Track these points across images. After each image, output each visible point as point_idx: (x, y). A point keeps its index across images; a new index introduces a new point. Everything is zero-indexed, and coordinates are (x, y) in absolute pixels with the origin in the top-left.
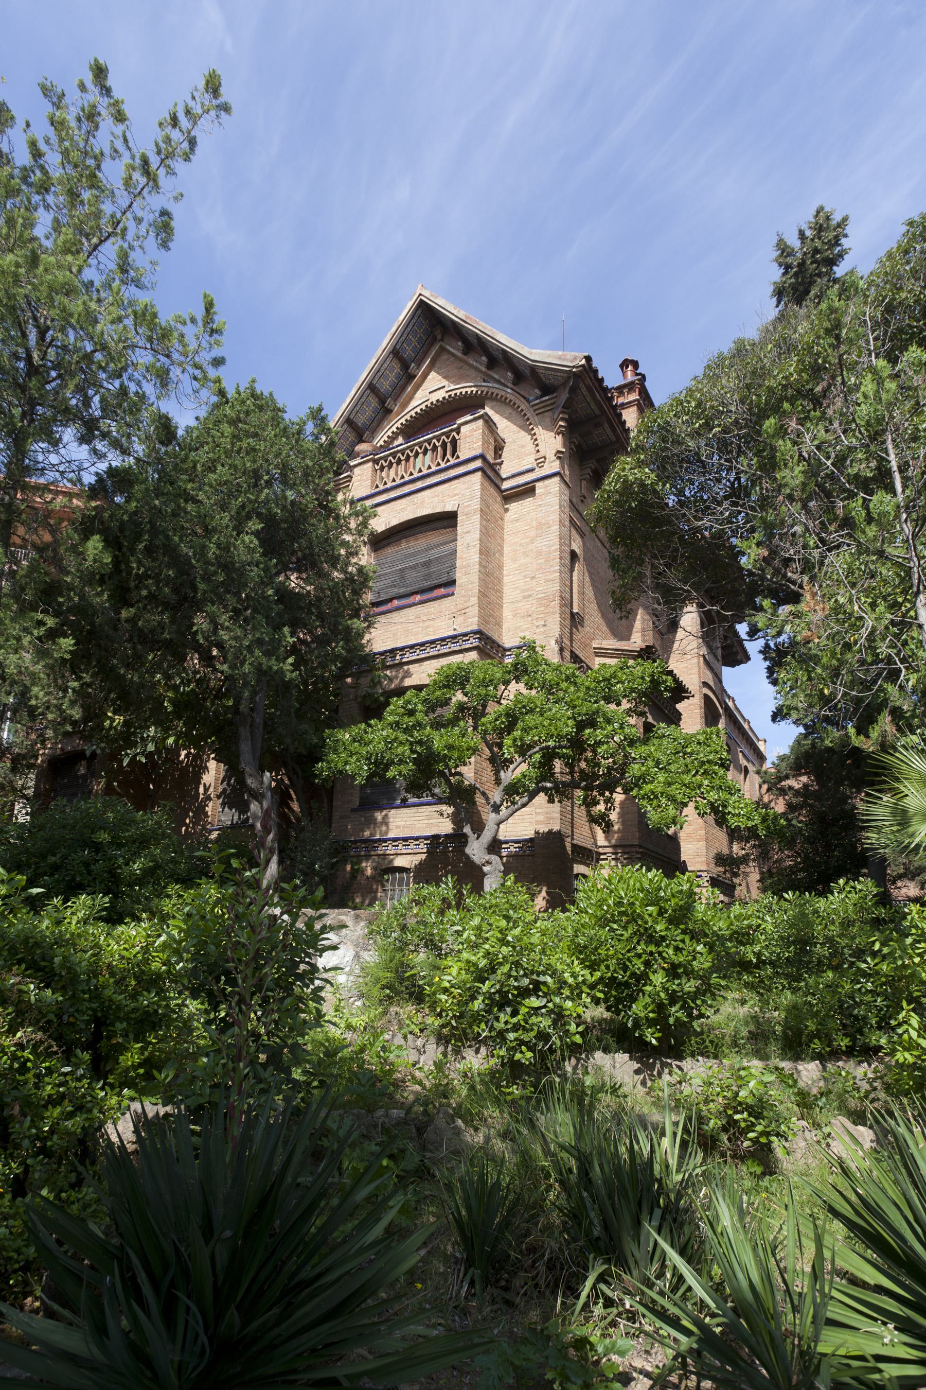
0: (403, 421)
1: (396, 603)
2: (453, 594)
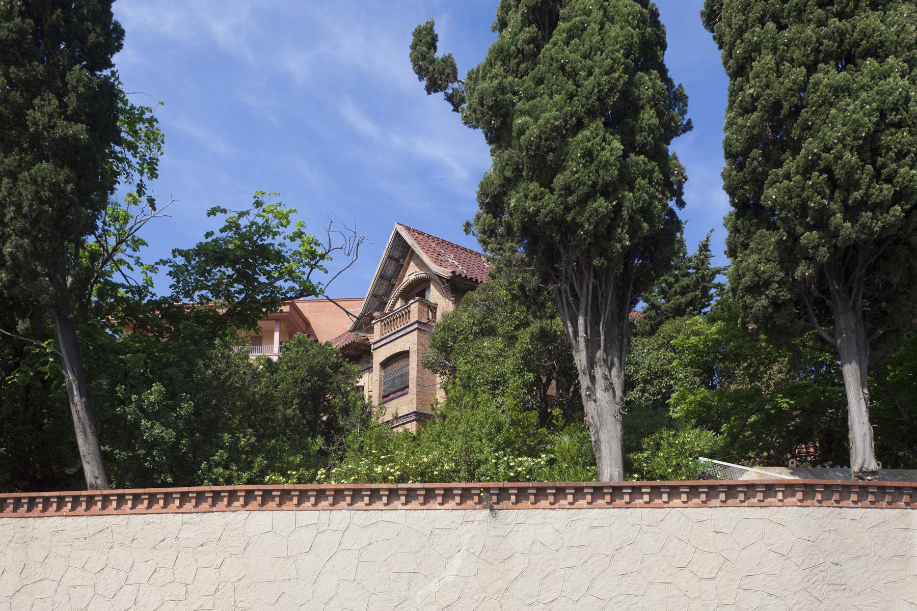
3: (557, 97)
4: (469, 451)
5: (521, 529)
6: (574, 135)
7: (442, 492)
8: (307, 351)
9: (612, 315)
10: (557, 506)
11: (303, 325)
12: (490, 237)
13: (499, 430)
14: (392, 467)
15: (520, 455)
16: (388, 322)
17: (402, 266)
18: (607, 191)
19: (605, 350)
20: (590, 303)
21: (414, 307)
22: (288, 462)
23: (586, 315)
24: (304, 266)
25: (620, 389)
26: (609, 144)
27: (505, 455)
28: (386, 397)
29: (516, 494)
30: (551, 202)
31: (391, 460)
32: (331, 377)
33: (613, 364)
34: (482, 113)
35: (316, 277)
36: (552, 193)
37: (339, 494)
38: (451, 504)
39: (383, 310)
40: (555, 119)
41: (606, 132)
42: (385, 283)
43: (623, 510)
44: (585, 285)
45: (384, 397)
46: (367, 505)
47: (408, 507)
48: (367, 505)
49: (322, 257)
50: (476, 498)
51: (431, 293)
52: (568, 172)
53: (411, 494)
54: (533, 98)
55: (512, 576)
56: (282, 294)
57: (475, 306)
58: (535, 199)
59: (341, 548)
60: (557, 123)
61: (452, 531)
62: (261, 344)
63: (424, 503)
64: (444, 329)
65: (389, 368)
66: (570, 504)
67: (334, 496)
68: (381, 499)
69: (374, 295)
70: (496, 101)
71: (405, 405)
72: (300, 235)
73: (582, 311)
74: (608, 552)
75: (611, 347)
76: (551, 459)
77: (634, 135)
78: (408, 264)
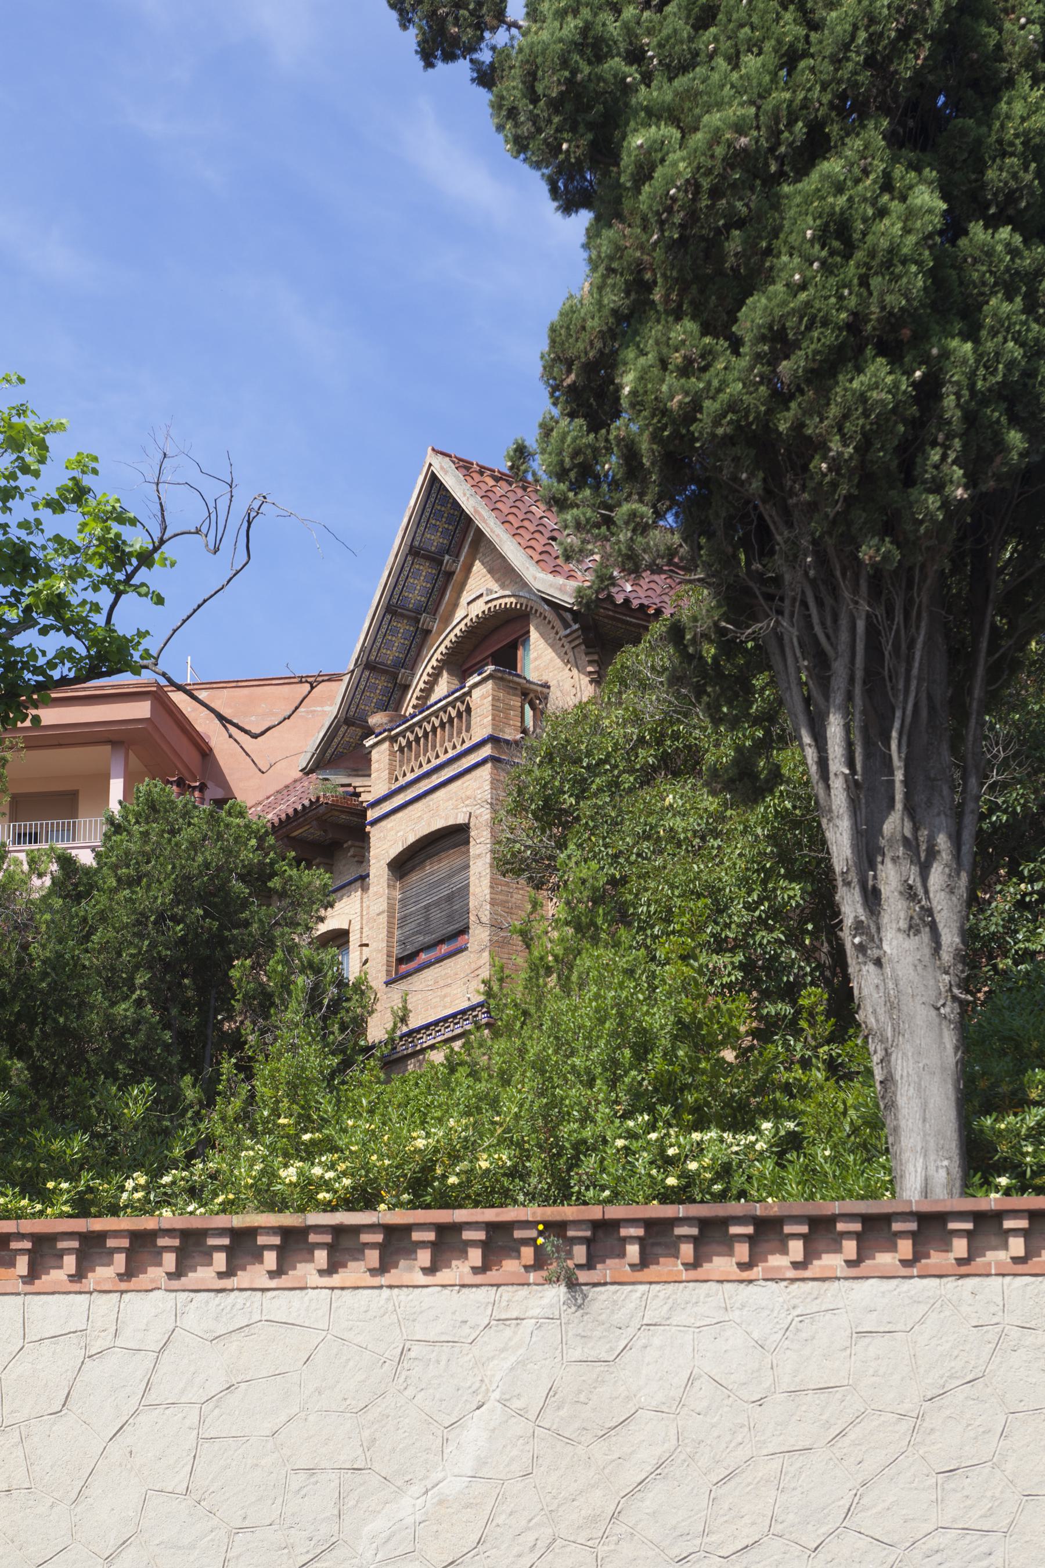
0: (447, 643)
1: (423, 957)
2: (466, 949)
3: (751, 62)
4: (551, 1116)
5: (656, 1341)
6: (802, 172)
7: (431, 1236)
8: (173, 832)
9: (932, 708)
10: (757, 1272)
11: (192, 757)
12: (577, 486)
13: (642, 1051)
14: (332, 1167)
15: (700, 1125)
16: (409, 743)
17: (450, 575)
18: (896, 340)
19: (910, 810)
20: (859, 674)
21: (483, 696)
22: (50, 1158)
23: (847, 714)
24: (96, 588)
25: (955, 926)
26: (903, 199)
27: (652, 1127)
28: (406, 962)
29: (640, 1240)
30: (733, 377)
31: (329, 1146)
32: (245, 904)
33: (932, 854)
34: (534, 119)
35: (131, 616)
36: (737, 353)
37: (191, 1245)
38: (459, 1270)
39: (398, 707)
40: (740, 129)
41: (895, 160)
42: (403, 627)
43: (950, 1283)
44: (844, 622)
45: (400, 961)
46: (221, 1275)
47: (336, 1280)
48: (221, 1275)
49: (146, 559)
50: (528, 1253)
51: (533, 654)
52: (778, 288)
53: (346, 1242)
54: (685, 68)
55: (632, 1476)
56: (37, 670)
57: (644, 686)
58: (686, 370)
59: (152, 1398)
60: (744, 141)
61: (461, 1345)
62: (74, 814)
63: (383, 1268)
64: (549, 757)
65: (414, 877)
66: (796, 1265)
67: (130, 1253)
68: (259, 1258)
69: (369, 664)
70: (570, 82)
71: (449, 988)
72: (79, 494)
73: (838, 698)
74: (905, 1407)
75: (929, 804)
76: (791, 1134)
77: (981, 168)
78: (468, 569)
